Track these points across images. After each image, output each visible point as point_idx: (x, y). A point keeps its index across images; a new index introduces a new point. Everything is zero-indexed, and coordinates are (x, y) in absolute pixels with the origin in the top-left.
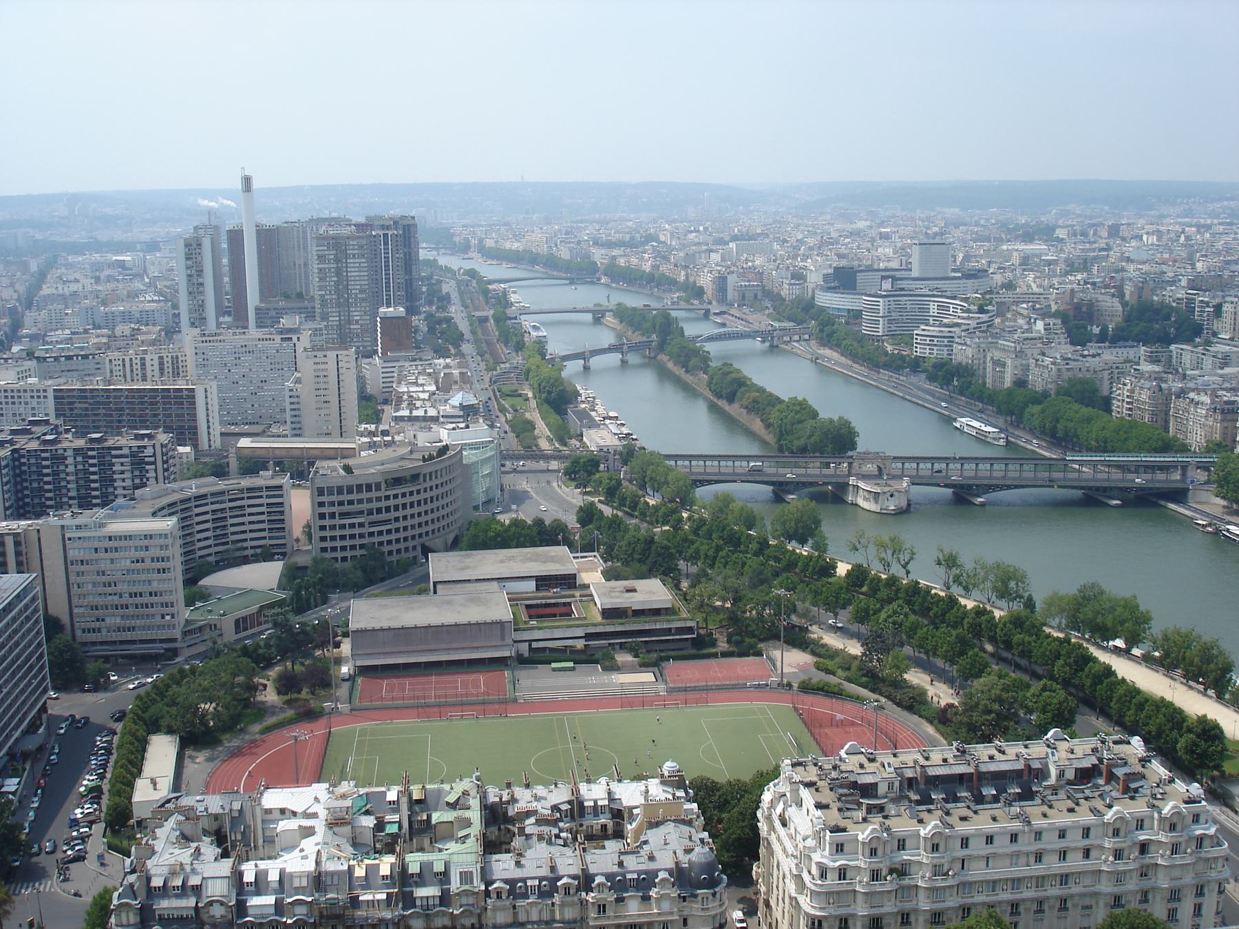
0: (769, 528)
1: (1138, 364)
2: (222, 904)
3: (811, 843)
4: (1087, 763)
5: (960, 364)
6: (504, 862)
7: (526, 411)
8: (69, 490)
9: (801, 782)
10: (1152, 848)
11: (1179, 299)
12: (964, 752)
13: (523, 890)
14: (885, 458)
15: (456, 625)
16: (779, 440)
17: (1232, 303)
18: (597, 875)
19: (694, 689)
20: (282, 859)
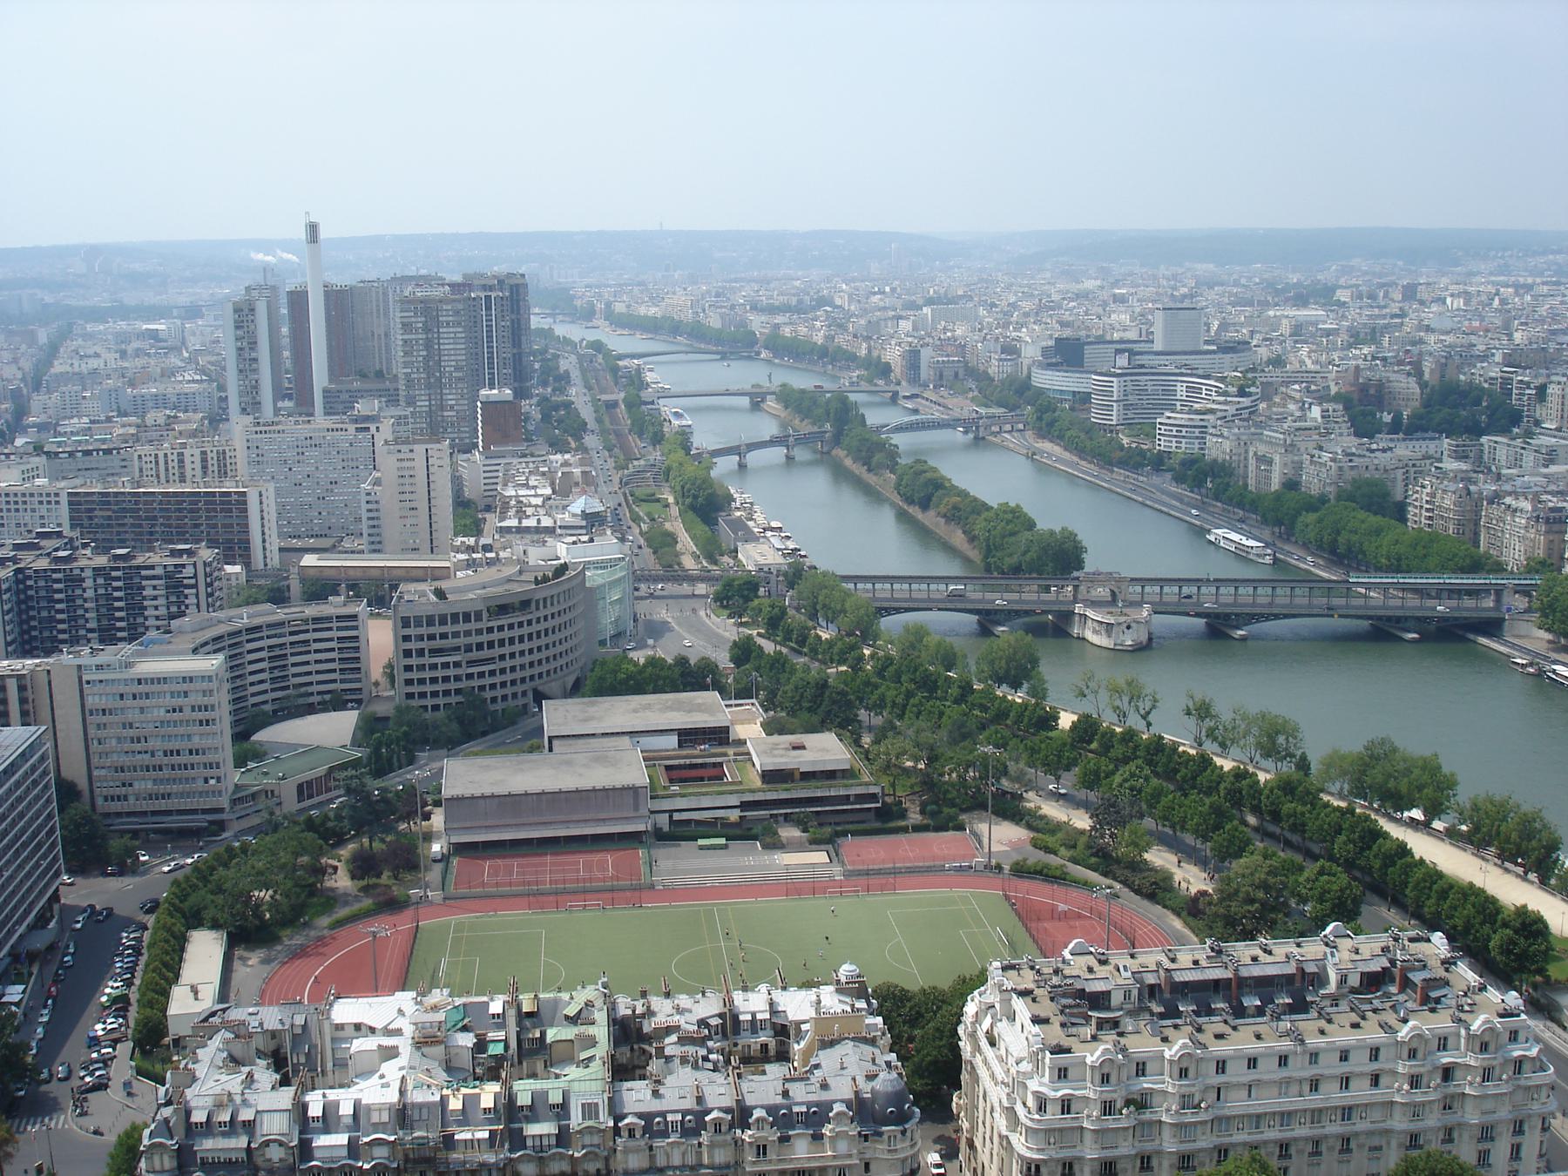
0: (973, 668)
1: (1440, 460)
2: (281, 1144)
3: (1026, 1067)
4: (1376, 966)
5: (1215, 461)
6: (638, 1091)
7: (665, 520)
8: (87, 621)
9: (1014, 990)
10: (1458, 1073)
11: (1492, 379)
12: (1220, 952)
13: (662, 1127)
14: (1120, 580)
15: (577, 791)
16: (986, 557)
17: (1559, 383)
18: (756, 1107)
19: (879, 872)
20: (357, 1087)
